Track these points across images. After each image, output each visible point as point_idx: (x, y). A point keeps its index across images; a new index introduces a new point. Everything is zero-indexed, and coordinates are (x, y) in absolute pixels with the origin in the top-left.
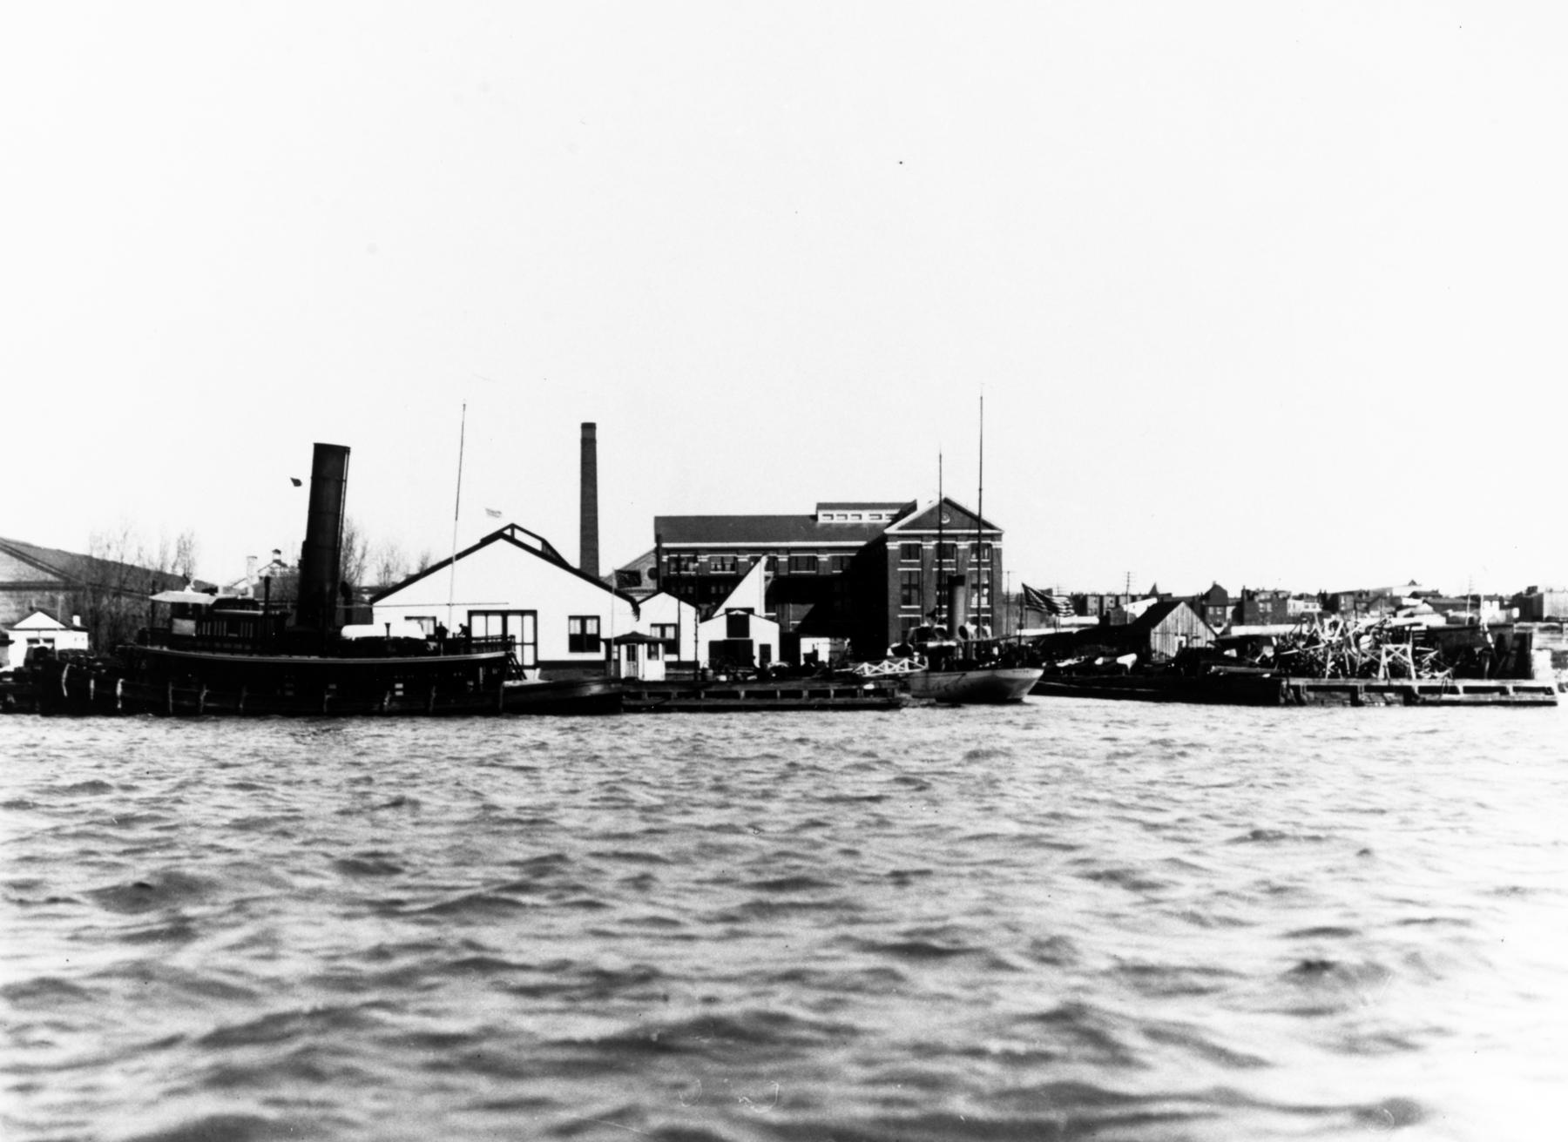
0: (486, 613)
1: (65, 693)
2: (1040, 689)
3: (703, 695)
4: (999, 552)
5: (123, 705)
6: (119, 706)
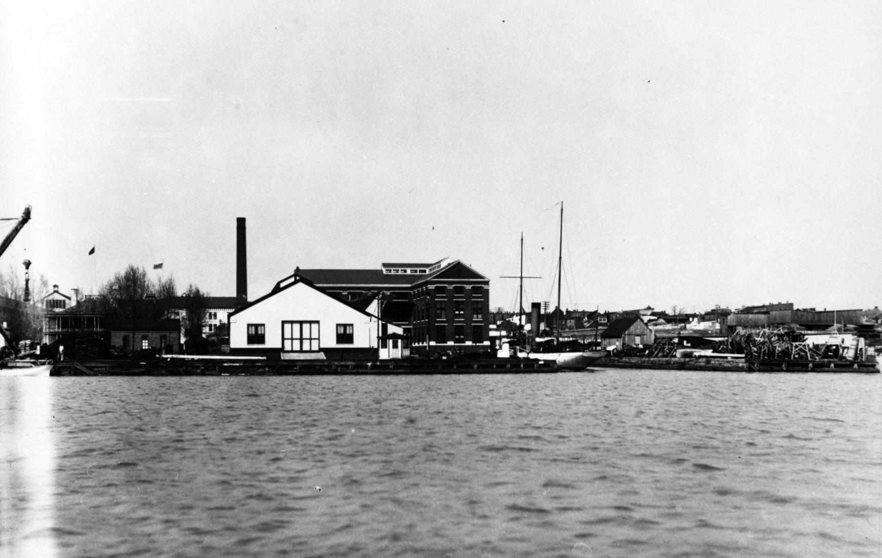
0: (292, 322)
1: (184, 348)
2: (540, 360)
3: (455, 367)
4: (488, 291)
5: (58, 349)
6: (61, 348)
